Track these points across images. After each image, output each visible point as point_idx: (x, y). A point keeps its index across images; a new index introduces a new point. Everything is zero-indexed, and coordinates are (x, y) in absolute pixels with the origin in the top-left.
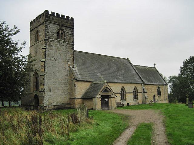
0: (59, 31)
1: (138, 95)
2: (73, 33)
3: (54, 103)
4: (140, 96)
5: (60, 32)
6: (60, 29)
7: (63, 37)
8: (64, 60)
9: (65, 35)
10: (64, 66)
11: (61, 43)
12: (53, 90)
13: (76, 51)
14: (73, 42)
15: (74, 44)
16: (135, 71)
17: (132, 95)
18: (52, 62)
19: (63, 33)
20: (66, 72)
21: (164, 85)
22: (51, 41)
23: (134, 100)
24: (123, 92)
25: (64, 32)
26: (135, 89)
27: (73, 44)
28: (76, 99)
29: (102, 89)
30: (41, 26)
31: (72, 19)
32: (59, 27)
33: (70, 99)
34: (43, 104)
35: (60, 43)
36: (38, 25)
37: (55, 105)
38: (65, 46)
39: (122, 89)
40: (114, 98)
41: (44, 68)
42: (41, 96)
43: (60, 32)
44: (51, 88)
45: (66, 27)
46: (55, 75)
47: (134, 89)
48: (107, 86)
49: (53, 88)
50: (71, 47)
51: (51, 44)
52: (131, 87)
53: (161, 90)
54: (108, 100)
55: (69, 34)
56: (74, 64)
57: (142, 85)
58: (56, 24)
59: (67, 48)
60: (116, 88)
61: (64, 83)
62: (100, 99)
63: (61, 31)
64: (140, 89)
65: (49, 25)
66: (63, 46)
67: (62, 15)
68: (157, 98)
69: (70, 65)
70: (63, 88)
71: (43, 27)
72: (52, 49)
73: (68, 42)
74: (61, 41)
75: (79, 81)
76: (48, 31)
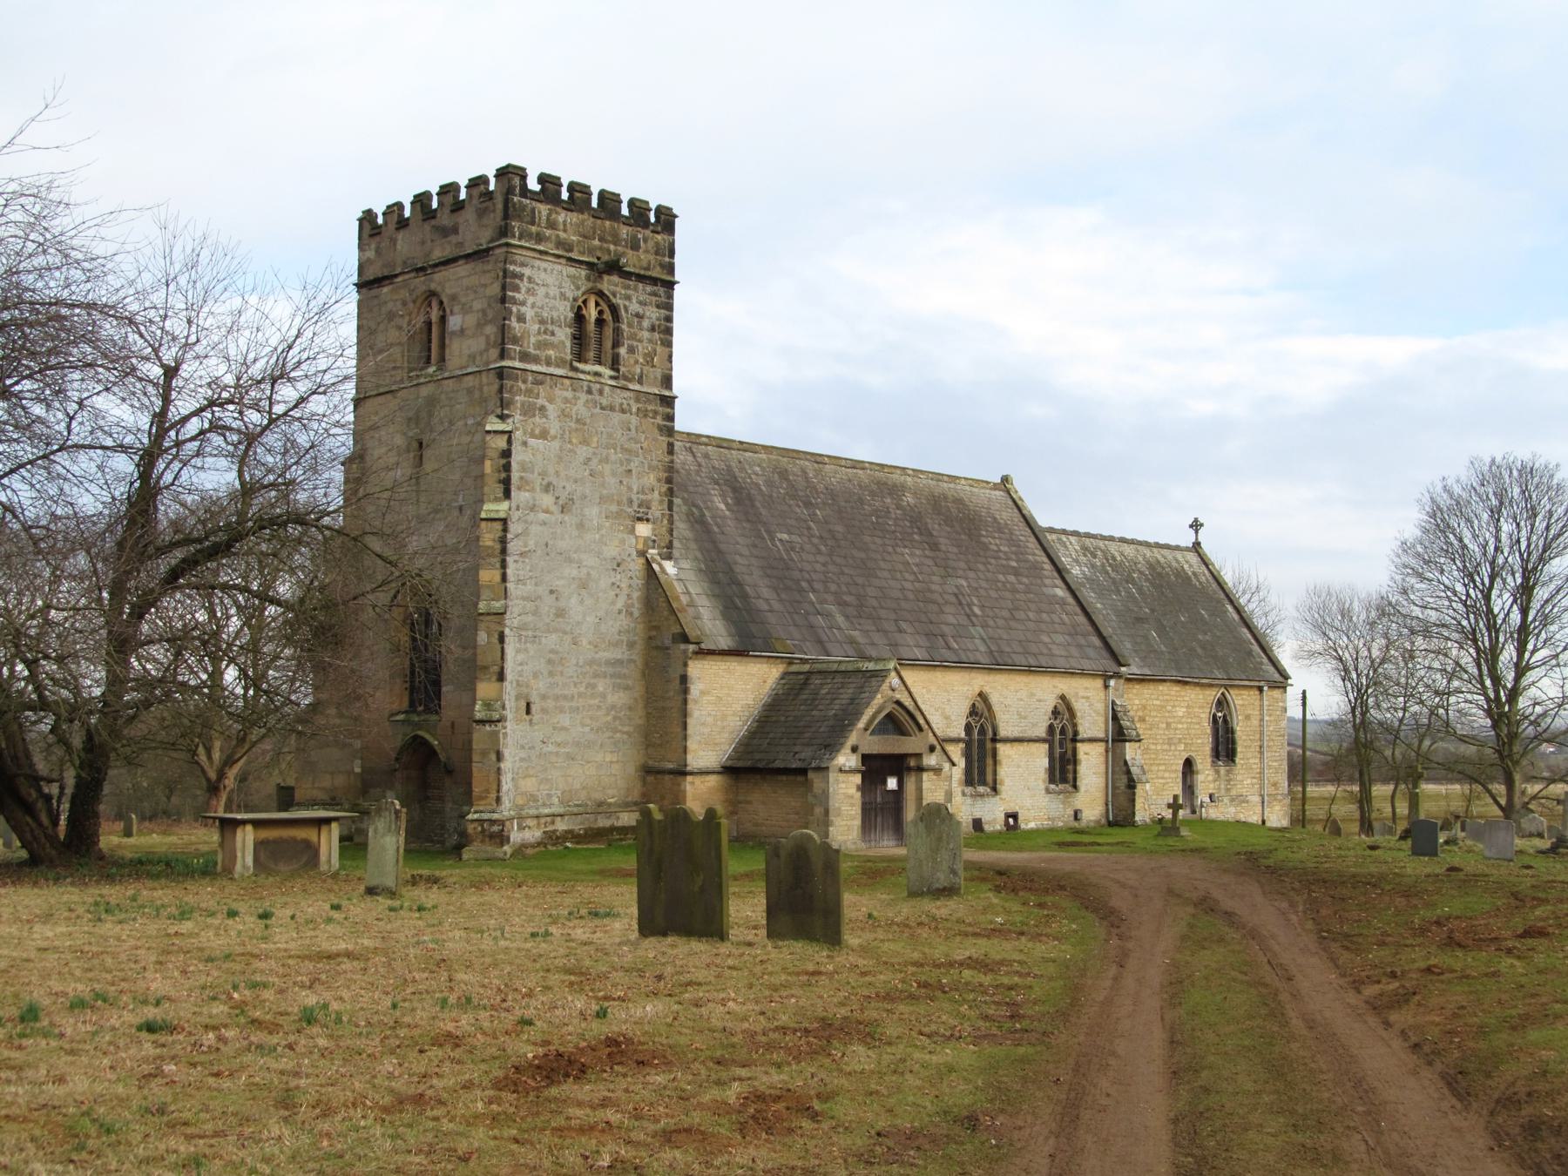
0: (585, 302)
1: (1081, 755)
2: (669, 319)
3: (550, 796)
4: (1091, 763)
5: (592, 313)
6: (589, 291)
7: (608, 344)
8: (614, 508)
9: (617, 332)
10: (611, 551)
11: (596, 387)
12: (544, 711)
13: (694, 439)
14: (667, 381)
15: (676, 390)
16: (1058, 582)
17: (1038, 758)
18: (544, 523)
19: (607, 316)
20: (626, 591)
21: (1260, 689)
22: (540, 379)
23: (1048, 791)
24: (982, 731)
25: (614, 310)
26: (1064, 711)
27: (667, 393)
28: (691, 773)
29: (869, 713)
30: (462, 269)
31: (666, 220)
32: (588, 278)
33: (648, 771)
34: (498, 800)
35: (589, 392)
36: (438, 254)
37: (554, 810)
38: (623, 411)
39: (973, 712)
40: (937, 771)
41: (504, 565)
42: (484, 753)
43: (592, 313)
44: (534, 698)
45: (627, 275)
46: (561, 613)
47: (1056, 713)
48: (898, 696)
49: (544, 697)
50: (656, 413)
51: (540, 402)
52: (1032, 695)
53: (1241, 730)
54: (900, 783)
55: (646, 323)
56: (671, 531)
57: (1106, 687)
58: (570, 259)
59: (634, 420)
60: (942, 699)
61: (608, 663)
62: (858, 779)
63: (597, 304)
64: (1092, 721)
65: (527, 271)
66: (612, 409)
67: (602, 194)
68: (1206, 779)
69: (646, 539)
70: (603, 696)
71: (486, 279)
72: (544, 435)
73: (640, 382)
74: (597, 374)
75: (711, 653)
76: (523, 309)
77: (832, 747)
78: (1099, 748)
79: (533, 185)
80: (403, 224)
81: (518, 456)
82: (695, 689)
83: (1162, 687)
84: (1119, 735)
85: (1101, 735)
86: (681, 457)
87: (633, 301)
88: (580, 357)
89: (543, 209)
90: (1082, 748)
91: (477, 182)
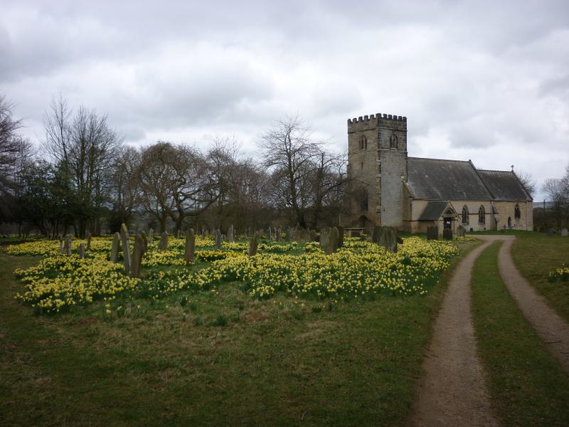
4: (488, 218)
5: (393, 139)
17: (477, 218)
26: (482, 209)
30: (370, 132)
31: (405, 119)
33: (404, 221)
36: (365, 129)
39: (464, 209)
43: (393, 139)
60: (458, 206)
68: (513, 222)
77: (439, 217)
78: (486, 211)
79: (382, 116)
80: (357, 122)
81: (382, 166)
82: (413, 206)
83: (504, 203)
84: (494, 212)
85: (489, 212)
86: (409, 163)
87: (400, 135)
88: (391, 146)
89: (384, 121)
90: (486, 215)
91: (372, 116)
